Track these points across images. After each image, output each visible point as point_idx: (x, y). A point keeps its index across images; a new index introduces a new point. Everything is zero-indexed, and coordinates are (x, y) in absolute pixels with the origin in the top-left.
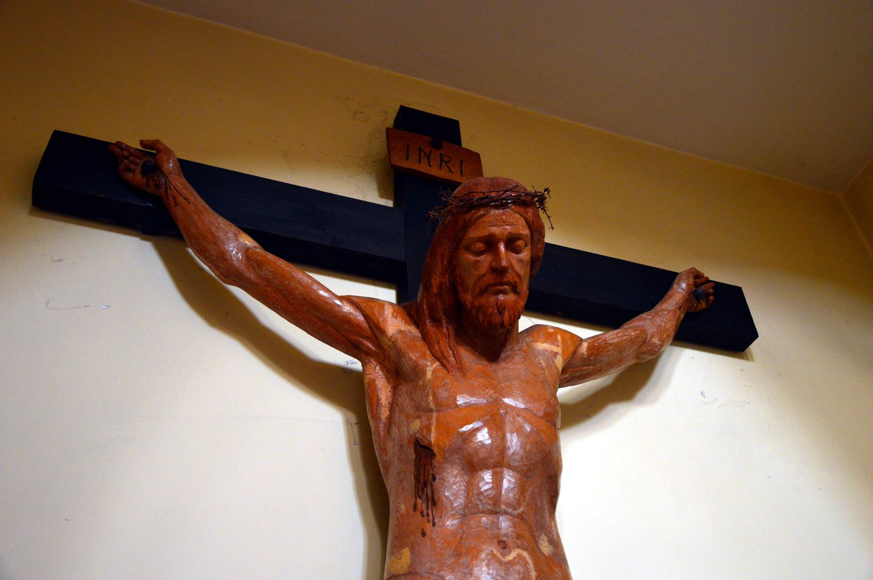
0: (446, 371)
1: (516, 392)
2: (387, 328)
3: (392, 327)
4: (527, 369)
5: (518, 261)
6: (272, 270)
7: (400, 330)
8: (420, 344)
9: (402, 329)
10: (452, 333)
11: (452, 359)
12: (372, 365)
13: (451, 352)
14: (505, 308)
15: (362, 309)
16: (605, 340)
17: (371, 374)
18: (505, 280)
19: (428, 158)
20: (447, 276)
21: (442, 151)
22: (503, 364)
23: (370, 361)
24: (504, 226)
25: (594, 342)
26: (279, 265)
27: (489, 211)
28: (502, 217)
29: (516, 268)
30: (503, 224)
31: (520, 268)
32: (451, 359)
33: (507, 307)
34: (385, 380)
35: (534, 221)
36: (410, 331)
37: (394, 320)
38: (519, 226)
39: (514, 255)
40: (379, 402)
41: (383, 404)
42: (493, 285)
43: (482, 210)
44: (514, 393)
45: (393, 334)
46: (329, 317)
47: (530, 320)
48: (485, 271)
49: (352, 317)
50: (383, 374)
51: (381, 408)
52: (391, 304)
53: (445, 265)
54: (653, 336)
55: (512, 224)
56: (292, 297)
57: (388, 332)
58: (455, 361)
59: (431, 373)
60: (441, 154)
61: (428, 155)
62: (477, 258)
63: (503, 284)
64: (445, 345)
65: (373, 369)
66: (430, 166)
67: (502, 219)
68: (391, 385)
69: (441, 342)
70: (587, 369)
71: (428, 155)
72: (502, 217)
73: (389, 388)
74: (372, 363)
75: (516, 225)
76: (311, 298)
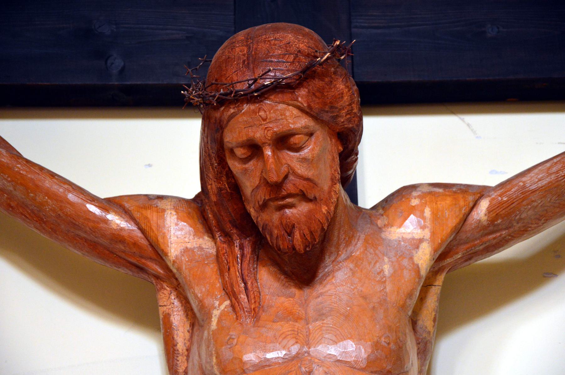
0: (235, 317)
1: (327, 336)
2: (169, 249)
3: (176, 246)
4: (353, 290)
5: (299, 161)
6: (9, 179)
7: (187, 248)
8: (211, 270)
9: (189, 246)
10: (248, 250)
11: (243, 296)
12: (165, 292)
13: (243, 285)
14: (293, 226)
15: (136, 221)
16: (524, 187)
17: (165, 306)
18: (284, 193)
20: (224, 179)
22: (319, 289)
23: (162, 288)
24: (265, 125)
26: (17, 172)
27: (240, 108)
28: (260, 114)
29: (299, 172)
30: (263, 122)
31: (307, 169)
32: (242, 296)
33: (296, 225)
34: (183, 312)
35: (312, 105)
36: (201, 248)
38: (287, 120)
39: (292, 154)
40: (175, 348)
41: (180, 350)
43: (232, 107)
44: (323, 339)
45: (177, 257)
46: (96, 237)
47: (463, 120)
48: (257, 183)
49: (124, 234)
50: (180, 305)
51: (177, 357)
53: (216, 167)
55: (276, 120)
56: (44, 214)
57: (169, 255)
58: (246, 300)
59: (216, 320)
62: (244, 166)
63: (284, 198)
64: (236, 274)
65: (167, 298)
67: (260, 116)
68: (189, 322)
69: (232, 269)
70: (494, 238)
72: (260, 114)
73: (188, 327)
74: (165, 289)
75: (282, 119)
76: (67, 215)
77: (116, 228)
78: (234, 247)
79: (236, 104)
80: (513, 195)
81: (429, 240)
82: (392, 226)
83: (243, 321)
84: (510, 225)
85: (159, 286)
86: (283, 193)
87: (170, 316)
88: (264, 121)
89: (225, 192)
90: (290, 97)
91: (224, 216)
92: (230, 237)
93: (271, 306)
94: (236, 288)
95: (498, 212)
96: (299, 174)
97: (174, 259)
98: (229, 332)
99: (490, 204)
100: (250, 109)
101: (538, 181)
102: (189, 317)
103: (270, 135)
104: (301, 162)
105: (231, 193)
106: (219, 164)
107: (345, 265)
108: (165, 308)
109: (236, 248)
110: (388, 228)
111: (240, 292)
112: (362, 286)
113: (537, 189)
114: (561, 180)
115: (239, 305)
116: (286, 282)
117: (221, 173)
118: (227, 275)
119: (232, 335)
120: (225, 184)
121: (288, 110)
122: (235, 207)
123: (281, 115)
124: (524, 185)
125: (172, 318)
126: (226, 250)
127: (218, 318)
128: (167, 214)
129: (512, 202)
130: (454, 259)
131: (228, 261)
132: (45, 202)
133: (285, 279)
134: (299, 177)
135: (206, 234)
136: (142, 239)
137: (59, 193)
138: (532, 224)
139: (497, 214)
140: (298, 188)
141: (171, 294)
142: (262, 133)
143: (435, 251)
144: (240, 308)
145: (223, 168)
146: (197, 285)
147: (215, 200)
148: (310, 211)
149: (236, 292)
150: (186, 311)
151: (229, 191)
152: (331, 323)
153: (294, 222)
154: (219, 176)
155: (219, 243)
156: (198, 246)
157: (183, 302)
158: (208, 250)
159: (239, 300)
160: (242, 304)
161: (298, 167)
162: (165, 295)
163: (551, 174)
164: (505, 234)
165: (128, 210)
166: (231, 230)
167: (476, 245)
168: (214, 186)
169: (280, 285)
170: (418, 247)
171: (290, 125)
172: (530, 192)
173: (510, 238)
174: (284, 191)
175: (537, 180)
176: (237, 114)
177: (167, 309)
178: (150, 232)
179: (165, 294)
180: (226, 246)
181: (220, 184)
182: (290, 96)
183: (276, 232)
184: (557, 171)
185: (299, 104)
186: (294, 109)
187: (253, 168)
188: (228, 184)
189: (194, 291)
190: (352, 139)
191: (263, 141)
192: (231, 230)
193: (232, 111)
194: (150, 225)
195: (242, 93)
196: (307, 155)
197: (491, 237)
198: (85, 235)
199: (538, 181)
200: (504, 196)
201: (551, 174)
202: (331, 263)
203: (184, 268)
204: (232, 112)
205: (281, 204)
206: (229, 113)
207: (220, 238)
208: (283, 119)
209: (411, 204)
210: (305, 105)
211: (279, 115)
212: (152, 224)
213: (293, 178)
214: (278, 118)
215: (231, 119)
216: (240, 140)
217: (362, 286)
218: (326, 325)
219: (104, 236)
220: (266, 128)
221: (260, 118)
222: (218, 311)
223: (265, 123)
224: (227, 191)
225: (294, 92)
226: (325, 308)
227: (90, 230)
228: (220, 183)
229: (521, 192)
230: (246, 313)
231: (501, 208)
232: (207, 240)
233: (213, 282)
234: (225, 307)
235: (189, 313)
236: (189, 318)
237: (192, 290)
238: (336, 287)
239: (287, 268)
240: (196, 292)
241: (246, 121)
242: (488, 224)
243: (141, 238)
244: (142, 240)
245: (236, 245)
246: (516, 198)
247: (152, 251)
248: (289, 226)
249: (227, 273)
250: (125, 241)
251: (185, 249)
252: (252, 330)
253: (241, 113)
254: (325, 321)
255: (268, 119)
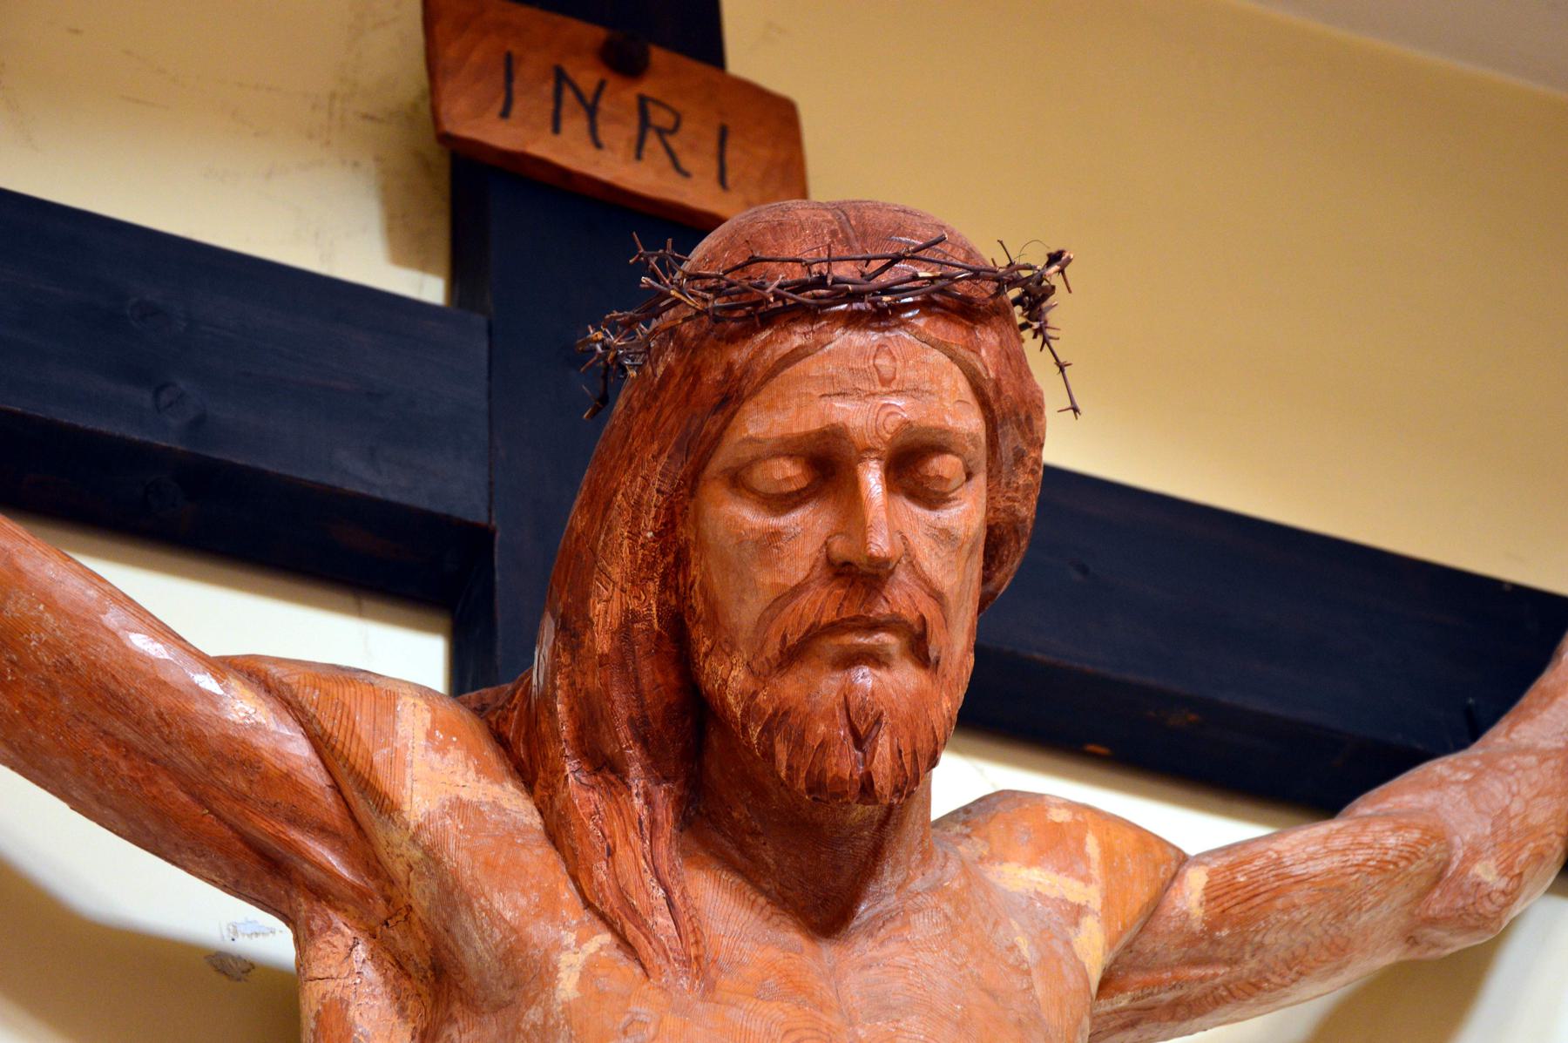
0: (638, 970)
9: (465, 795)
10: (666, 814)
12: (337, 940)
14: (878, 721)
16: (1278, 862)
19: (592, 111)
20: (652, 587)
21: (647, 87)
23: (329, 926)
25: (1231, 867)
27: (824, 337)
28: (878, 362)
29: (926, 565)
30: (879, 388)
36: (496, 806)
37: (435, 757)
39: (919, 511)
42: (835, 628)
43: (798, 329)
45: (429, 817)
48: (801, 575)
50: (380, 980)
52: (425, 693)
53: (643, 546)
54: (1474, 854)
57: (406, 808)
58: (673, 931)
59: (575, 978)
60: (643, 102)
61: (589, 100)
63: (874, 627)
64: (637, 864)
65: (341, 958)
66: (598, 145)
70: (1202, 979)
71: (589, 100)
72: (878, 362)
74: (338, 931)
75: (931, 393)
77: (241, 722)
78: (630, 796)
79: (812, 324)
80: (1258, 876)
81: (1100, 914)
82: (1004, 860)
83: (667, 981)
84: (1238, 956)
85: (320, 923)
86: (881, 611)
87: (348, 1004)
88: (883, 385)
89: (644, 627)
90: (964, 338)
91: (617, 703)
92: (613, 770)
93: (740, 964)
94: (638, 899)
95: (1226, 905)
96: (924, 572)
97: (421, 820)
98: (628, 1005)
99: (1208, 882)
100: (850, 341)
101: (1306, 860)
102: (408, 1012)
103: (892, 429)
104: (935, 538)
105: (659, 636)
106: (658, 535)
107: (933, 904)
108: (331, 985)
109: (636, 799)
110: (994, 864)
111: (652, 911)
112: (978, 965)
113: (1306, 877)
114: (1352, 874)
115: (650, 943)
116: (772, 914)
117: (652, 566)
118: (605, 868)
119: (637, 1014)
120: (650, 604)
121: (950, 373)
122: (660, 680)
123: (931, 381)
124: (1279, 858)
125: (353, 1012)
126: (596, 806)
127: (581, 973)
128: (405, 704)
129: (1252, 894)
130: (1112, 1004)
131: (607, 832)
132: (32, 619)
133: (768, 907)
134: (919, 582)
135: (509, 779)
136: (312, 765)
137: (86, 600)
138: (1274, 973)
139: (1223, 911)
140: (916, 609)
141: (354, 946)
142: (870, 417)
143: (1111, 944)
144: (654, 950)
145: (661, 553)
146: (500, 891)
147: (606, 651)
148: (921, 694)
149: (639, 909)
150: (398, 999)
151: (656, 626)
152: (920, 1031)
153: (882, 707)
154: (642, 575)
155: (575, 789)
156: (491, 800)
157: (390, 974)
158: (519, 816)
159: (651, 930)
160: (659, 941)
161: (926, 551)
162: (335, 950)
163: (1333, 852)
164: (1224, 974)
165: (281, 682)
166: (627, 748)
167: (1160, 983)
168: (615, 607)
169: (756, 918)
170: (1077, 924)
171: (947, 418)
172: (1292, 880)
173: (1225, 993)
174: (884, 603)
175: (1305, 856)
176: (807, 355)
177: (338, 986)
178: (347, 743)
179: (334, 946)
180: (596, 796)
181: (636, 601)
182: (965, 333)
183: (822, 728)
184: (1344, 850)
185: (980, 366)
186: (964, 379)
187: (799, 529)
188: (660, 604)
189: (491, 904)
190: (1008, 556)
191: (868, 442)
192: (629, 747)
193: (797, 341)
194: (350, 726)
195: (850, 287)
196: (955, 524)
197: (1196, 972)
198: (132, 737)
199: (1306, 860)
200: (1239, 872)
201: (1333, 852)
202: (894, 889)
203: (452, 846)
204: (796, 345)
205: (859, 645)
206: (786, 348)
207: (577, 775)
208: (933, 394)
209: (1049, 817)
210: (992, 375)
211: (927, 378)
212: (357, 724)
213: (906, 580)
214: (921, 387)
215: (782, 370)
216: (798, 429)
217: (978, 965)
218: (906, 1034)
219: (195, 740)
220: (884, 406)
221: (876, 376)
222: (579, 955)
223: (884, 390)
224: (651, 625)
225: (973, 328)
226: (894, 994)
227: (157, 719)
228: (639, 598)
229: (1274, 873)
230: (676, 965)
231: (1233, 898)
232: (512, 793)
233: (550, 886)
234: (601, 949)
235: (410, 1003)
236: (408, 1016)
237: (482, 901)
238: (915, 951)
239: (769, 883)
240: (496, 906)
241: (832, 378)
242: (1202, 931)
243: (309, 764)
244: (312, 769)
245: (635, 791)
246: (1264, 885)
247: (334, 805)
248: (867, 715)
249: (604, 862)
250: (259, 762)
251: (454, 800)
252: (699, 1006)
253: (820, 353)
254: (902, 1025)
255: (895, 382)
